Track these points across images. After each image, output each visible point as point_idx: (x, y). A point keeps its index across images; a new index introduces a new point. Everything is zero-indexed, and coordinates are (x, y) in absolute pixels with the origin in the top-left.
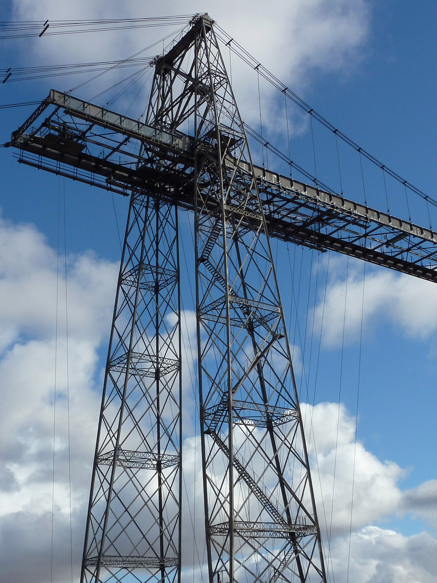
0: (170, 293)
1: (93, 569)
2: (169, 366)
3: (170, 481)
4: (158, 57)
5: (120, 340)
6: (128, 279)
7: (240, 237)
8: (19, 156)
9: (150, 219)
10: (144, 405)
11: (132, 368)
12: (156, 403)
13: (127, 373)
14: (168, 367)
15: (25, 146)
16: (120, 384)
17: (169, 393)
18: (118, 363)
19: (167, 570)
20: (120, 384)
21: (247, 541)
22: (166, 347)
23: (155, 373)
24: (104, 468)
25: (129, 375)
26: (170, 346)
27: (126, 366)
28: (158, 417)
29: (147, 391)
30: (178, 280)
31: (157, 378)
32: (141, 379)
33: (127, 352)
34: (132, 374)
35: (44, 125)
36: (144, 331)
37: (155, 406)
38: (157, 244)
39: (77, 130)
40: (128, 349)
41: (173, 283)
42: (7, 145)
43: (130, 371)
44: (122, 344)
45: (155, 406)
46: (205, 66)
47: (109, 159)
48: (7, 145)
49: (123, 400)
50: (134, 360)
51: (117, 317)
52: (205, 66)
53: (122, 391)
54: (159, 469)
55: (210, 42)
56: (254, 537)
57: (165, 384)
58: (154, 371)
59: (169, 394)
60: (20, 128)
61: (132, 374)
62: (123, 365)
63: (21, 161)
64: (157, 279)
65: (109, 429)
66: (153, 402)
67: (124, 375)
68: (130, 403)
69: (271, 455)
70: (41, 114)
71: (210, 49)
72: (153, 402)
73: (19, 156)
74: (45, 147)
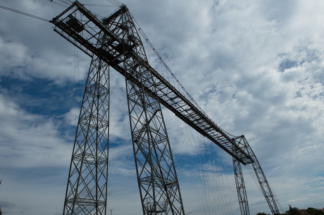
0: (105, 130)
1: (127, 20)
2: (102, 161)
3: (101, 210)
4: (316, 209)
5: (79, 147)
6: (83, 121)
7: (100, 97)
8: (54, 29)
9: (101, 77)
10: (90, 177)
11: (85, 160)
12: (95, 177)
13: (82, 162)
14: (102, 161)
15: (57, 25)
16: (79, 167)
17: (102, 173)
18: (78, 157)
19: (99, 207)
20: (79, 167)
21: (80, 206)
22: (101, 153)
23: (96, 163)
24: (70, 205)
25: (83, 163)
26: (103, 153)
27: (82, 159)
28: (97, 183)
29: (91, 171)
30: (108, 125)
31: (96, 166)
32: (89, 166)
33: (82, 152)
34: (85, 163)
35: (68, 16)
36: (92, 144)
37: (95, 178)
38: (98, 111)
39: (81, 23)
40: (83, 151)
41: (106, 127)
42: (50, 22)
43: (84, 161)
44: (80, 149)
45: (95, 178)
46: (70, 208)
47: (89, 41)
48: (50, 22)
49: (80, 174)
50: (86, 157)
51: (77, 137)
52: (70, 208)
53: (79, 170)
54: (97, 207)
55: (69, 212)
56: (83, 205)
57: (100, 169)
58: (95, 162)
59: (102, 173)
60: (57, 17)
61: (85, 163)
62: (80, 158)
63: (55, 30)
64: (97, 124)
65: (72, 187)
66: (94, 177)
67: (80, 162)
68: (84, 175)
69: (95, 174)
70: (62, 12)
71: (101, 79)
72: (94, 177)
73: (54, 29)
74: (65, 28)
